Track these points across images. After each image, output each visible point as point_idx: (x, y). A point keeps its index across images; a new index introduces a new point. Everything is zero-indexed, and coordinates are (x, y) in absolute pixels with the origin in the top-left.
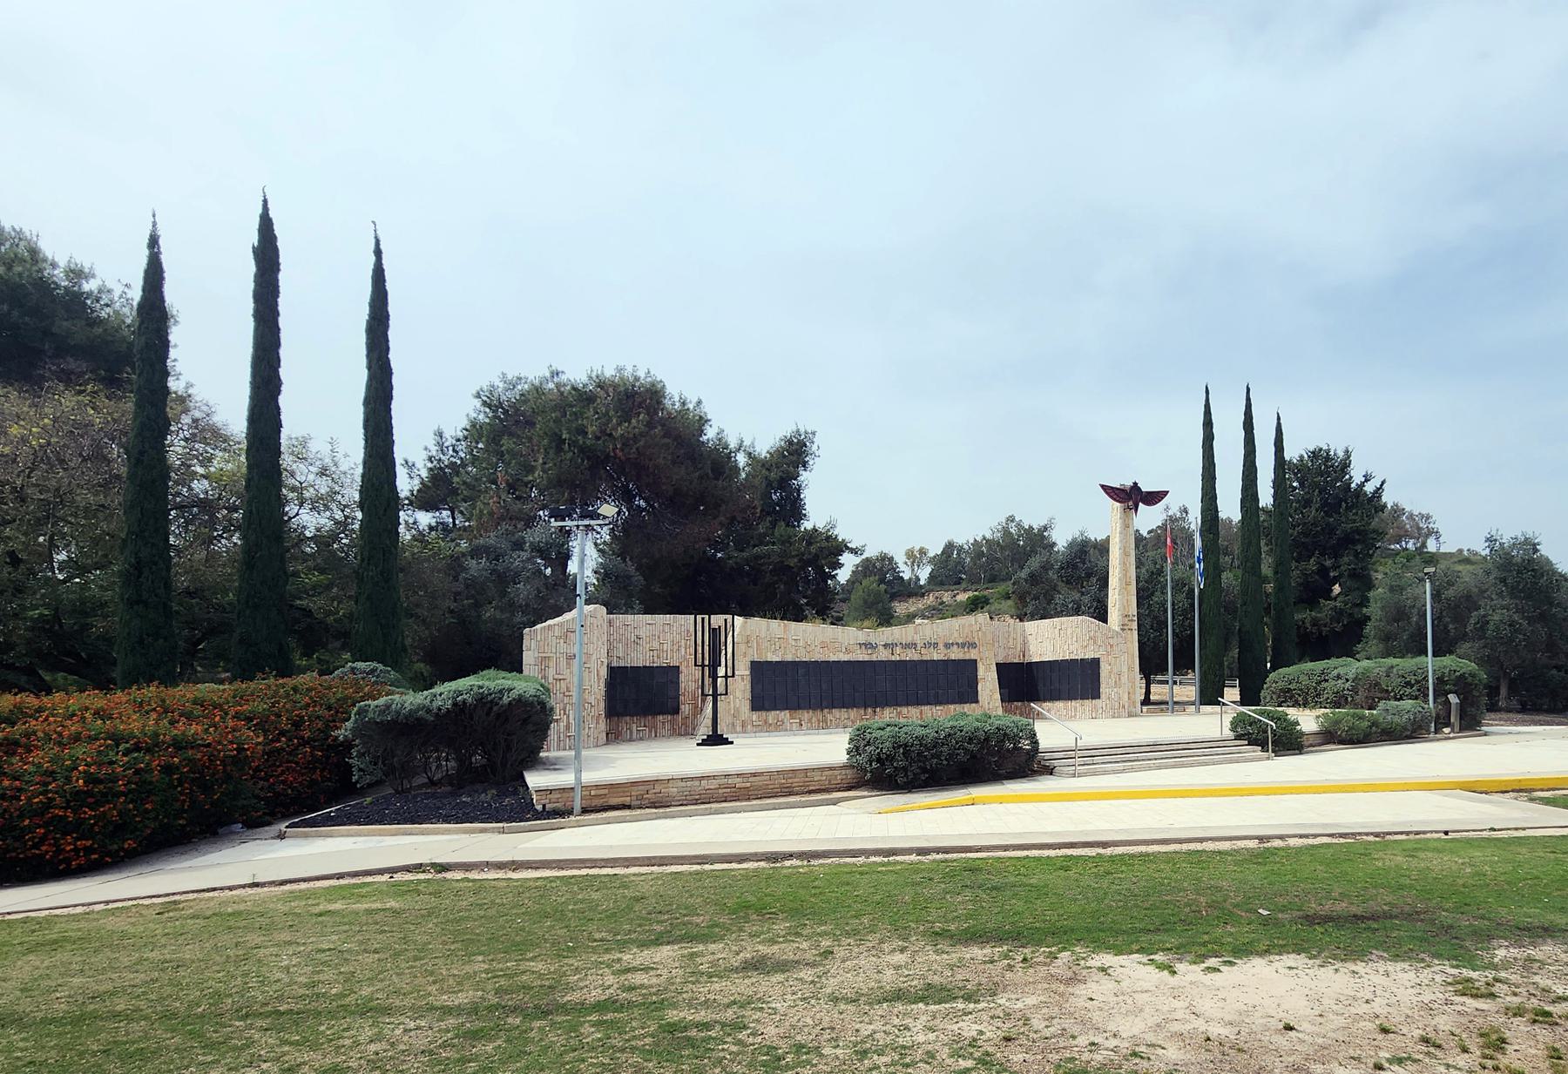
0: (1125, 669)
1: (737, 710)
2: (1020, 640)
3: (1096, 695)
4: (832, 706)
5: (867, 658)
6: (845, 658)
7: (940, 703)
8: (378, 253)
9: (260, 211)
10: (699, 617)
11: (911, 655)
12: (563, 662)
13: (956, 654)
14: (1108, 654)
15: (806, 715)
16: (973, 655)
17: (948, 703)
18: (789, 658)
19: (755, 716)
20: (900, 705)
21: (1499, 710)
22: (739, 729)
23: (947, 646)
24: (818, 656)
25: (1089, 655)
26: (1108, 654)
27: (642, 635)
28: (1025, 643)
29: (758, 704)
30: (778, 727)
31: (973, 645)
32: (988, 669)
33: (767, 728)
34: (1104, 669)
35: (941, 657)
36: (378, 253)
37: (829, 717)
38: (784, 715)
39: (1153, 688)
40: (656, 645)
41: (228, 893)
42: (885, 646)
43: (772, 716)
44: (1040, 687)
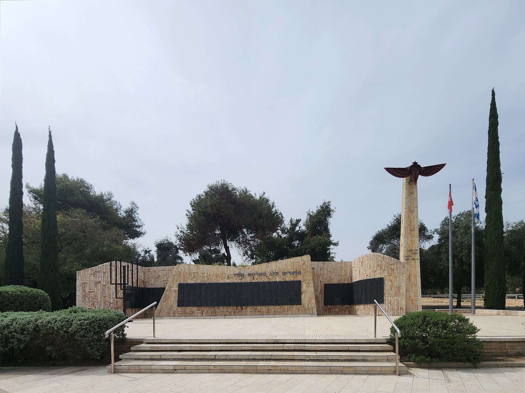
0: (403, 284)
1: (172, 306)
2: (349, 271)
3: (381, 301)
4: (219, 305)
5: (239, 281)
6: (228, 281)
7: (279, 305)
8: (50, 136)
9: (15, 130)
10: (114, 263)
11: (264, 279)
12: (93, 285)
13: (289, 278)
14: (390, 275)
15: (205, 309)
16: (299, 278)
17: (283, 304)
18: (199, 282)
19: (179, 309)
20: (256, 305)
21: (170, 316)
22: (171, 315)
23: (284, 274)
24: (214, 280)
25: (378, 276)
26: (390, 275)
27: (160, 274)
28: (351, 271)
29: (181, 303)
30: (191, 315)
31: (299, 273)
32: (308, 286)
33: (186, 315)
34: (387, 285)
35: (281, 280)
36: (50, 136)
37: (217, 310)
38: (195, 309)
39: (477, 301)
40: (165, 279)
41: (176, 353)
42: (249, 275)
43: (188, 309)
44: (355, 298)
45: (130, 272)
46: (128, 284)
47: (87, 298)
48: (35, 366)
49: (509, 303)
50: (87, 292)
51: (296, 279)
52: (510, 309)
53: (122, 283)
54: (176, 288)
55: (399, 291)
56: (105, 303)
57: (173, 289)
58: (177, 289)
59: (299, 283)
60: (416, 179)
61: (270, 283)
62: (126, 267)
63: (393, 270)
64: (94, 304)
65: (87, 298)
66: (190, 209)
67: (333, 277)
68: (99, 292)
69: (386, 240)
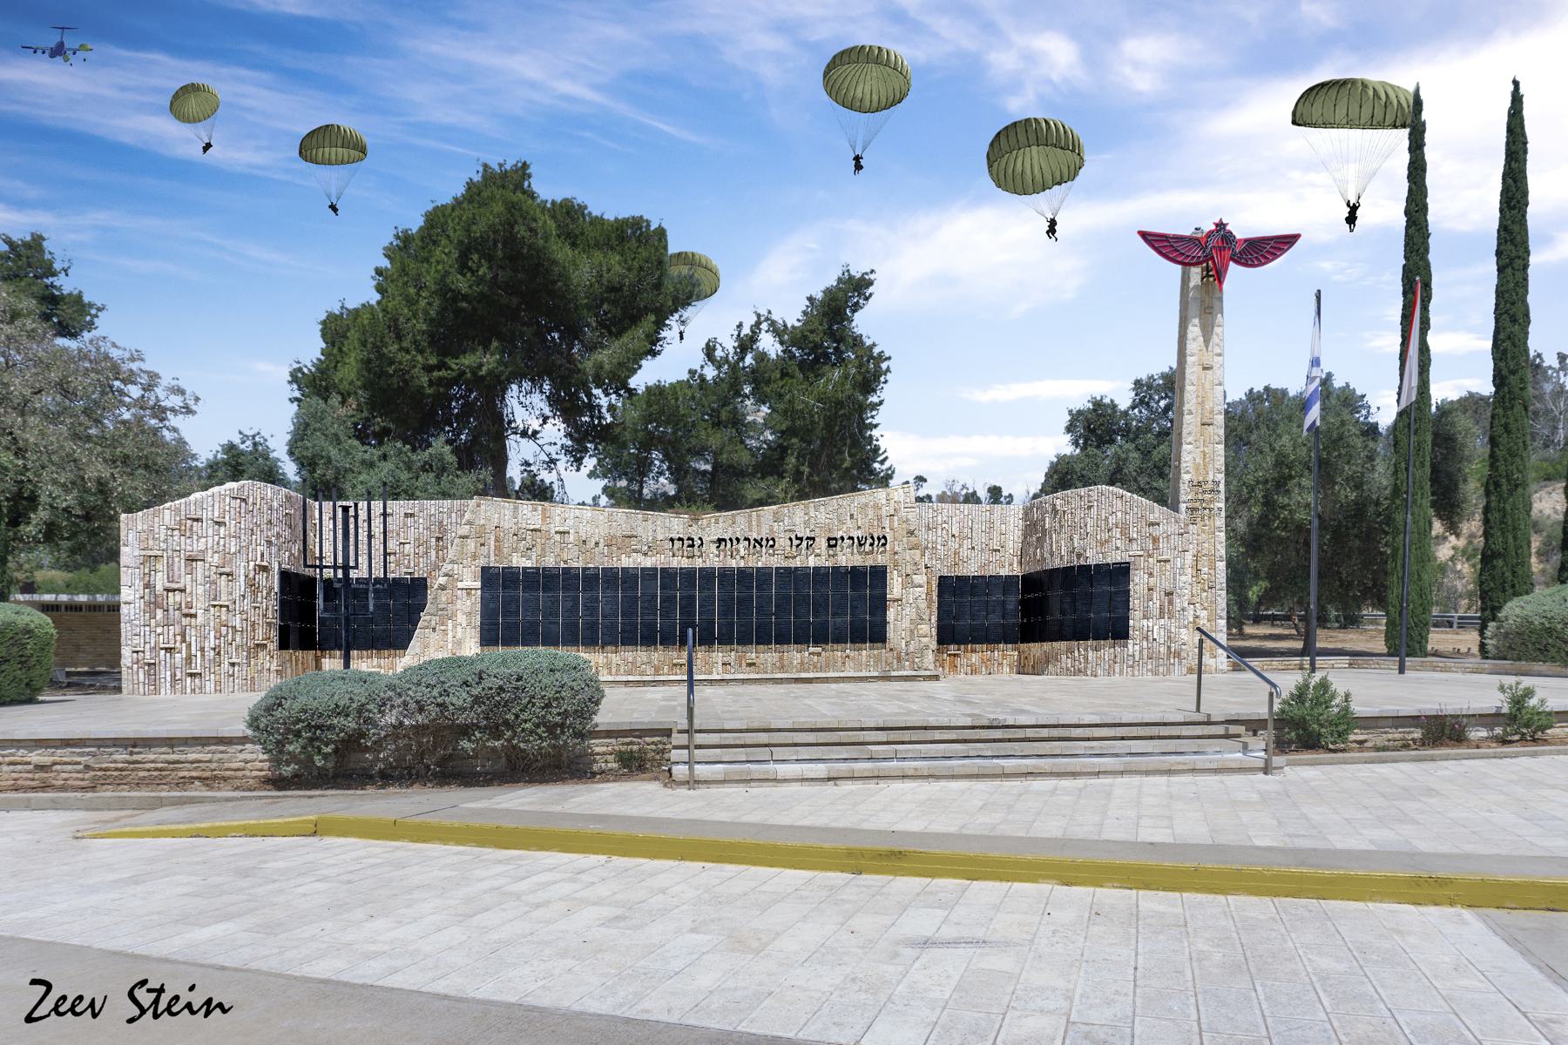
5: (685, 563)
12: (180, 564)
13: (847, 558)
29: (952, 633)
34: (1138, 582)
45: (363, 526)
46: (356, 567)
47: (159, 613)
48: (541, 782)
49: (1437, 639)
50: (159, 588)
51: (869, 562)
52: (1436, 654)
53: (340, 560)
54: (470, 580)
55: (1171, 603)
56: (218, 631)
57: (460, 585)
58: (478, 584)
59: (879, 574)
60: (1219, 277)
61: (789, 575)
62: (352, 512)
63: (1155, 540)
64: (183, 635)
65: (159, 613)
66: (385, 263)
67: (964, 553)
68: (200, 590)
69: (1119, 445)
